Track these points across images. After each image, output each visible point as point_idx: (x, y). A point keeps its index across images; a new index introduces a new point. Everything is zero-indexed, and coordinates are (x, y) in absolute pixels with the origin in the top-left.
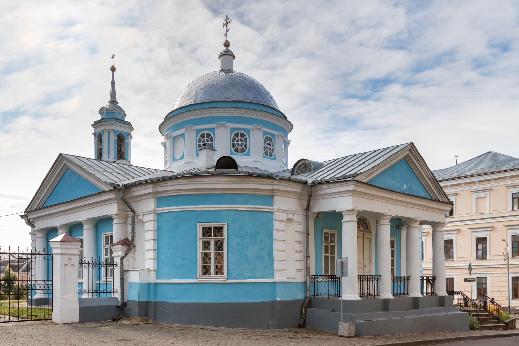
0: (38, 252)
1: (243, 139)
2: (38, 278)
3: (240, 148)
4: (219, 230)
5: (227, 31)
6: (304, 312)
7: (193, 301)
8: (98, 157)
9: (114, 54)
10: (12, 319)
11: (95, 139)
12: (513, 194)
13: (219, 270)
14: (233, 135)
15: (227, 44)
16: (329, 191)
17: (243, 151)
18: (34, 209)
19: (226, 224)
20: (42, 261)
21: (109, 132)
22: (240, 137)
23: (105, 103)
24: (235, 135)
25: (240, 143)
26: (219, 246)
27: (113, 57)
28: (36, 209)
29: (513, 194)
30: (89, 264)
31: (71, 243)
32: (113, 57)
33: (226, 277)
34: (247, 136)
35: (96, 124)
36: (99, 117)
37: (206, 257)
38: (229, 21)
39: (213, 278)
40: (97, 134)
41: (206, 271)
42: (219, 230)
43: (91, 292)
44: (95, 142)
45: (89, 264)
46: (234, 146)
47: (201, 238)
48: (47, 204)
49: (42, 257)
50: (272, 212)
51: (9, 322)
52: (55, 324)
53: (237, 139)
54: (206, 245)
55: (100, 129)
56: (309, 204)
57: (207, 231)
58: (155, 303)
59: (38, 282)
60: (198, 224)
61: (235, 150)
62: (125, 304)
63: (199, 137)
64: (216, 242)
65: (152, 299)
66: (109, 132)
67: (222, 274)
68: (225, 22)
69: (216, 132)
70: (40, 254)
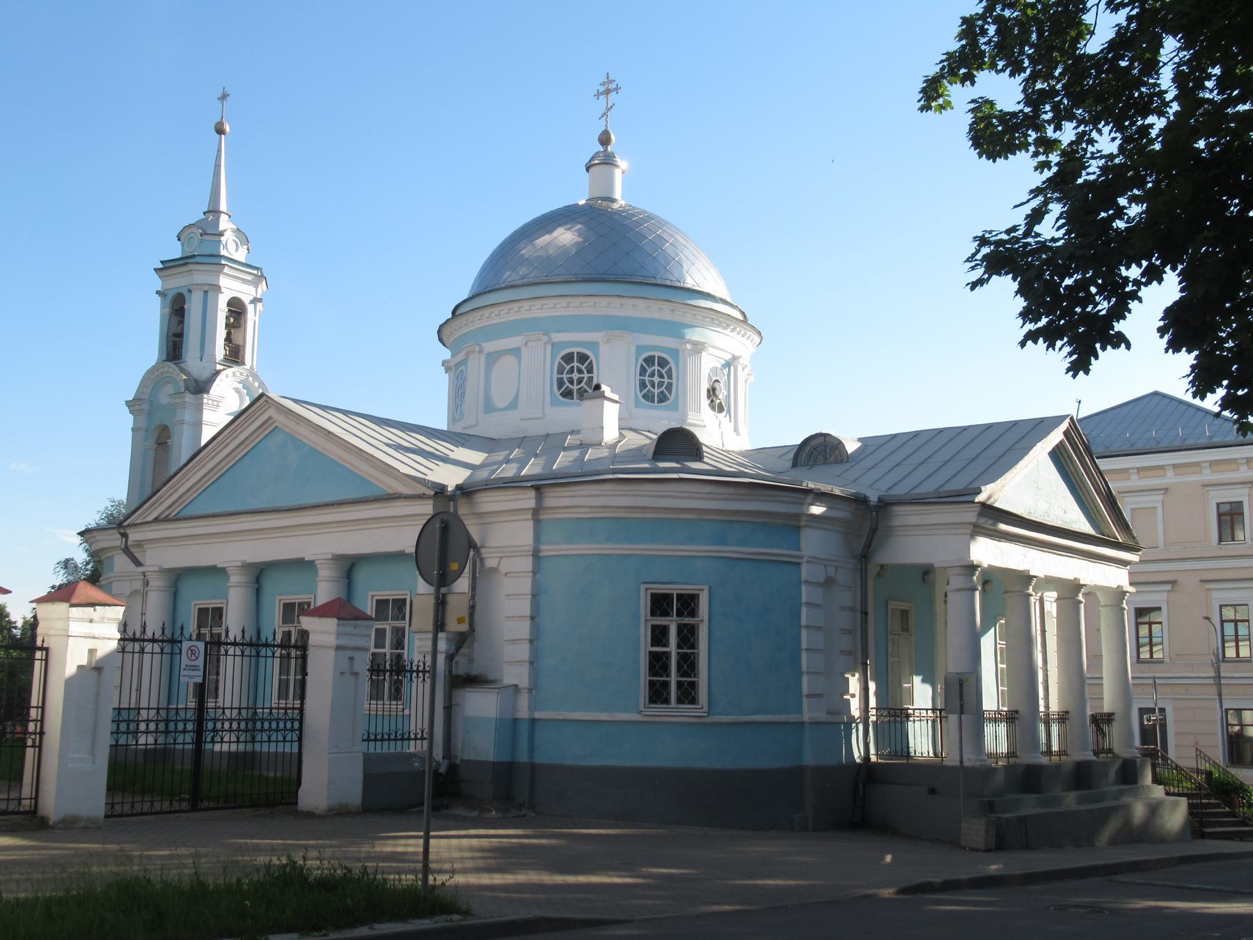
0: (149, 635)
1: (663, 372)
2: (228, 705)
3: (575, 364)
4: (688, 603)
5: (609, 110)
6: (861, 793)
7: (629, 764)
8: (168, 353)
9: (228, 90)
10: (176, 806)
11: (163, 307)
12: (1218, 504)
13: (688, 694)
14: (641, 361)
15: (605, 140)
16: (915, 520)
17: (663, 398)
18: (150, 518)
19: (706, 588)
20: (157, 657)
21: (206, 292)
22: (656, 367)
23: (195, 214)
24: (646, 360)
25: (575, 376)
26: (688, 636)
27: (224, 97)
28: (156, 520)
29: (1218, 504)
30: (424, 672)
31: (359, 622)
32: (224, 97)
33: (706, 709)
34: (672, 365)
35: (167, 267)
36: (175, 252)
37: (658, 663)
38: (613, 86)
39: (675, 712)
40: (171, 295)
41: (658, 694)
42: (688, 603)
43: (386, 737)
44: (162, 315)
45: (418, 671)
46: (643, 385)
47: (649, 617)
48: (183, 514)
49: (157, 648)
50: (799, 564)
51: (169, 812)
52: (310, 815)
53: (649, 371)
54: (659, 635)
55: (179, 282)
56: (868, 545)
57: (660, 604)
58: (533, 768)
59: (144, 714)
60: (643, 587)
61: (644, 396)
62: (453, 768)
63: (558, 359)
64: (680, 629)
65: (523, 757)
66: (206, 292)
67: (666, 701)
68: (602, 89)
69: (604, 350)
70: (153, 640)
